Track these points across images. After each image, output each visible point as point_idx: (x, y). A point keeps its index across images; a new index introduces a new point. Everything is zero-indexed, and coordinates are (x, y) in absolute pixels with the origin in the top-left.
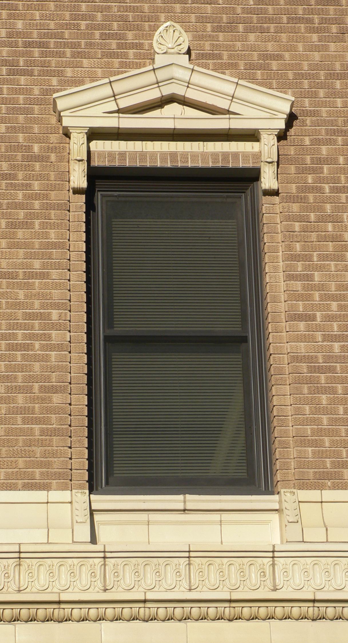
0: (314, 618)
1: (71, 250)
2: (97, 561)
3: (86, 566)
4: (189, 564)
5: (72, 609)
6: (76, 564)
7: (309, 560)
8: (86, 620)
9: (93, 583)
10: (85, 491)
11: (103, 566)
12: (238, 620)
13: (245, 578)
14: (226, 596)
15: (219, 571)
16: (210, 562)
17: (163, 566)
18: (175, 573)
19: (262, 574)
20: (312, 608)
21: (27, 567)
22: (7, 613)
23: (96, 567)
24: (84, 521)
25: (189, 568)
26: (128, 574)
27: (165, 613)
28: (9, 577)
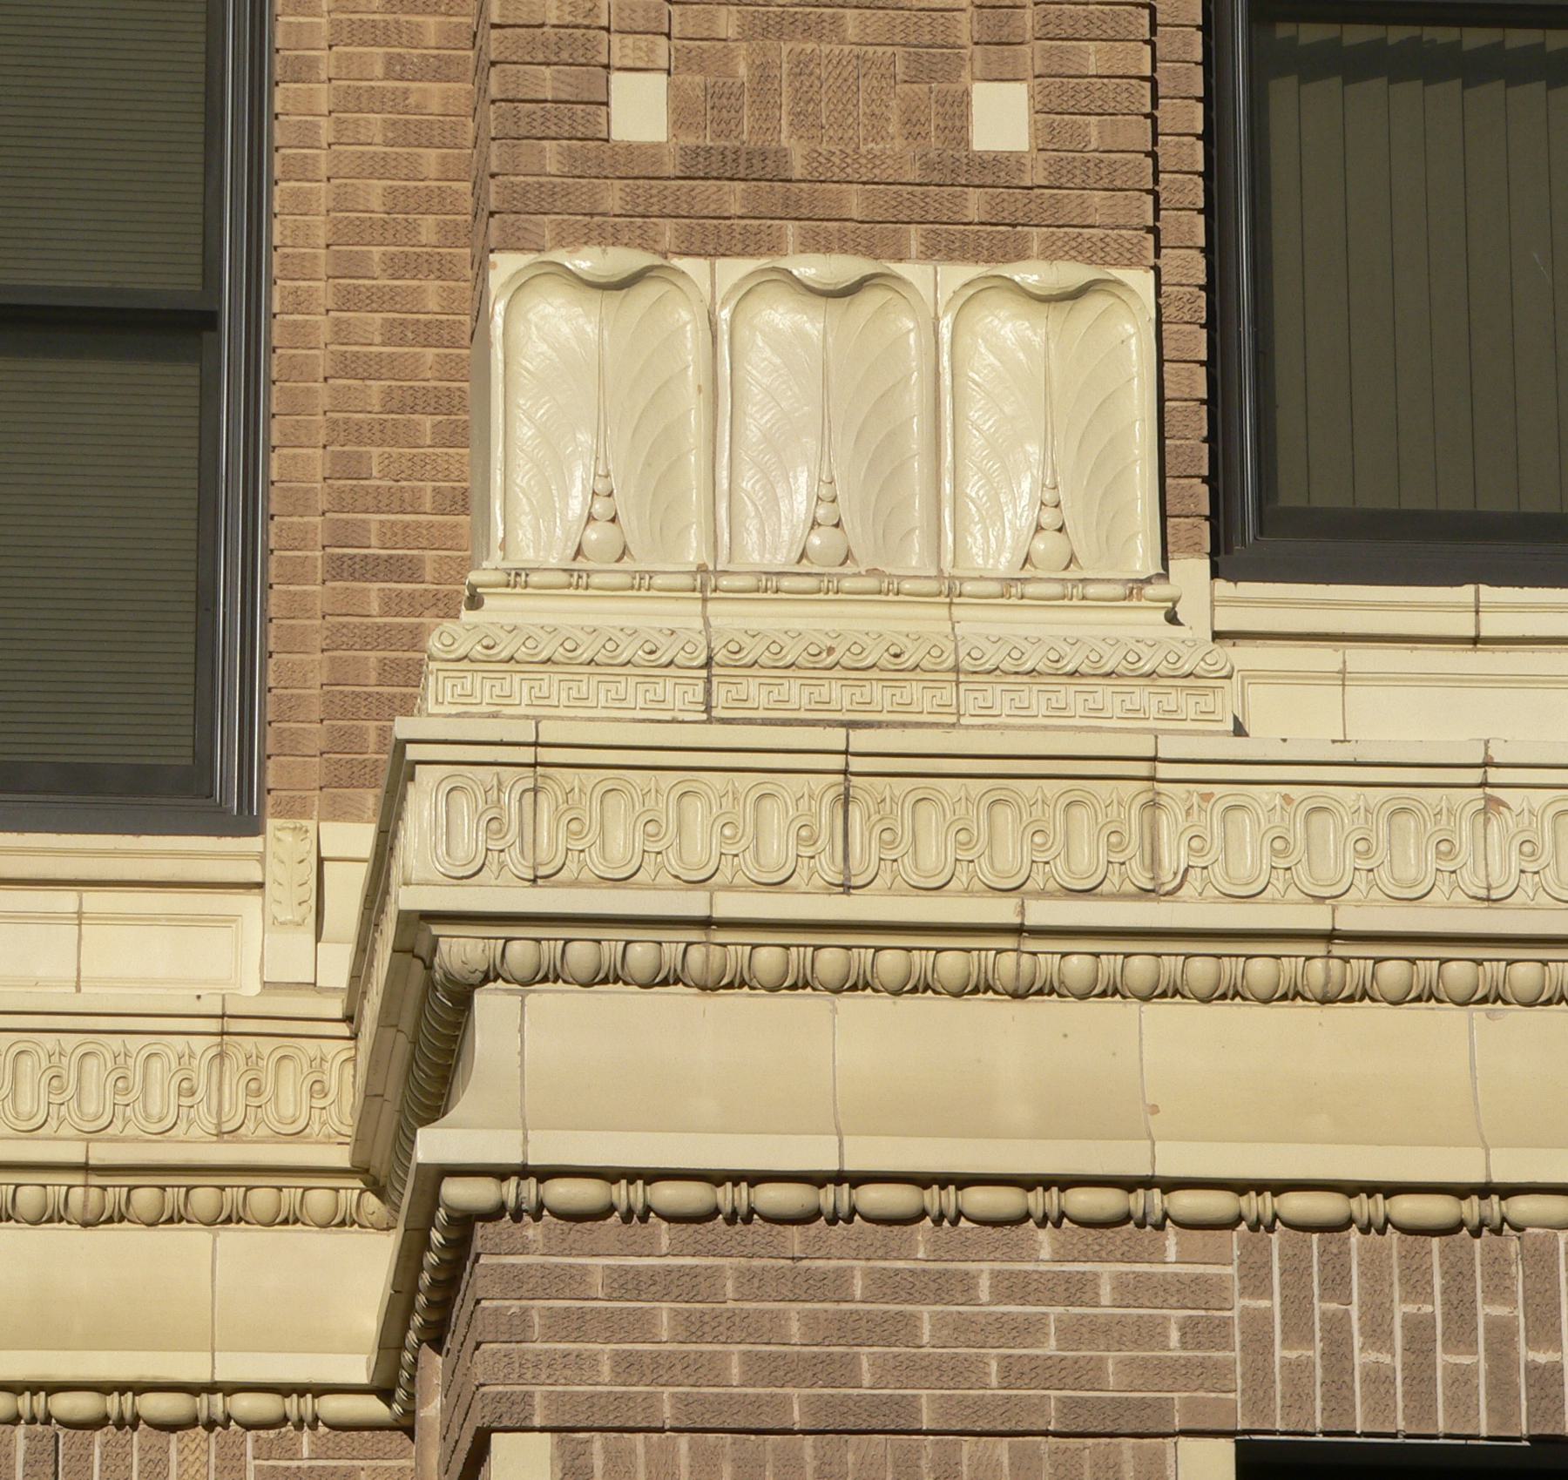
0: (89, 1217)
1: (675, 32)
2: (198, 1043)
3: (165, 1060)
4: (221, 1055)
5: (17, 1186)
6: (198, 1053)
7: (266, 1045)
8: (180, 1221)
9: (184, 1111)
10: (304, 822)
11: (217, 1061)
12: (290, 1227)
13: (262, 1100)
14: (74, 1154)
15: (115, 1075)
16: (153, 1049)
17: (75, 1059)
18: (45, 1079)
19: (253, 1085)
20: (80, 1191)
21: (242, 1062)
22: (29, 1197)
23: (131, 1062)
24: (298, 919)
25: (222, 1064)
26: (158, 1086)
27: (331, 1208)
28: (259, 1093)
